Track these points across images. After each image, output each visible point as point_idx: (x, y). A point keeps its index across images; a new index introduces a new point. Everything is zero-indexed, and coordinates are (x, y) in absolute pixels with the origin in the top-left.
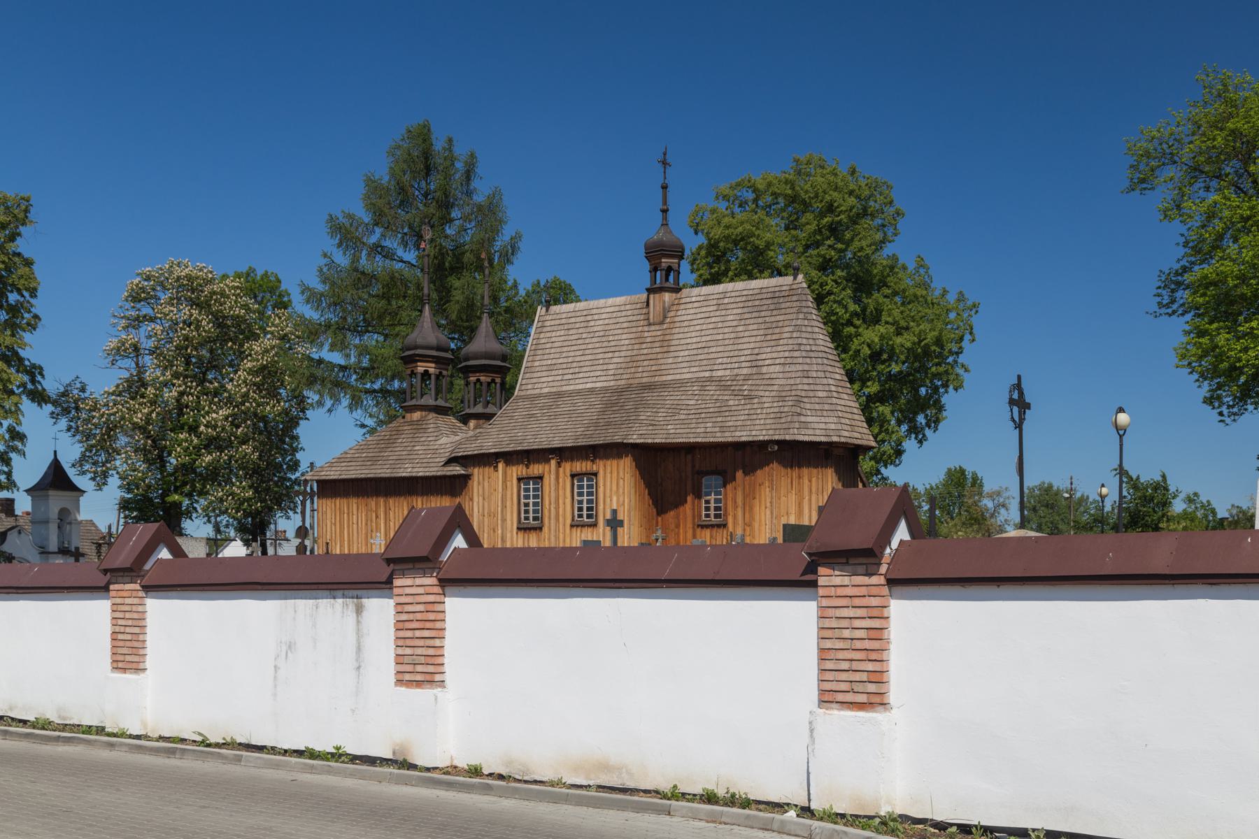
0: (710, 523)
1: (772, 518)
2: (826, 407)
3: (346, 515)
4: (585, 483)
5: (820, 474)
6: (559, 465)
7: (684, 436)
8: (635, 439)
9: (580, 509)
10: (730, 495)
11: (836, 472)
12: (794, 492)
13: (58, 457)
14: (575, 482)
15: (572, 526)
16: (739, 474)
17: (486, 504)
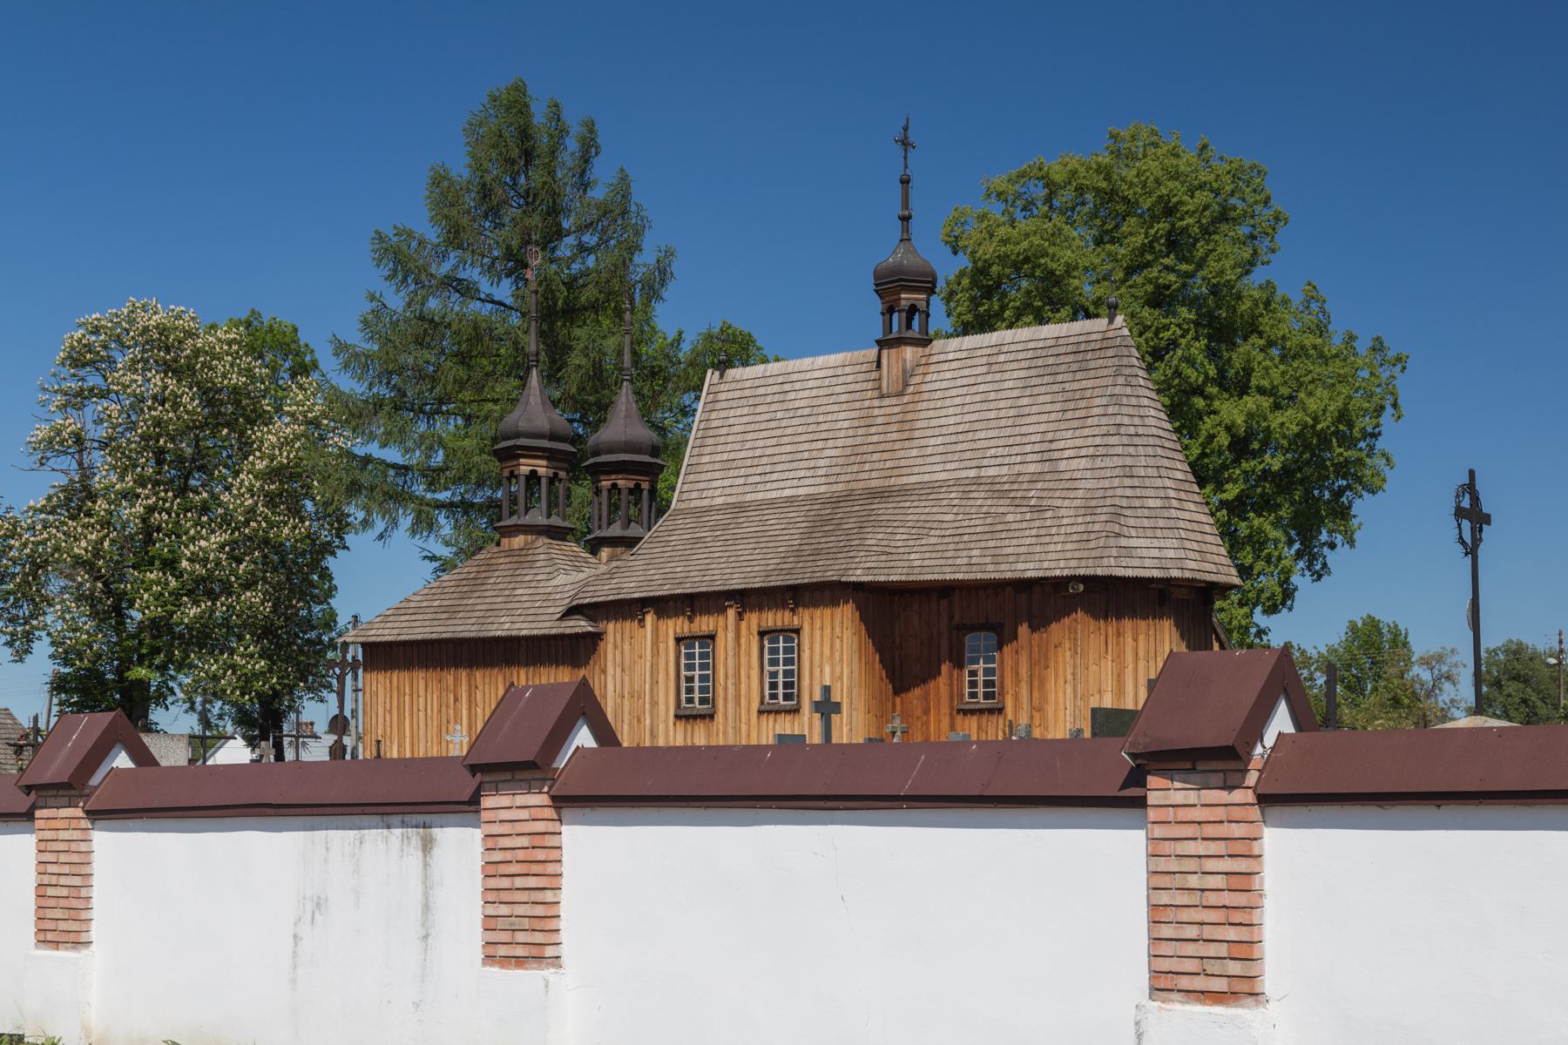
0: (977, 707)
1: (1075, 697)
2: (1161, 523)
3: (407, 697)
4: (781, 645)
5: (1152, 628)
6: (740, 616)
9: (774, 686)
10: (1008, 662)
11: (1177, 625)
12: (1110, 658)
15: (760, 712)
16: (1023, 630)
17: (626, 678)
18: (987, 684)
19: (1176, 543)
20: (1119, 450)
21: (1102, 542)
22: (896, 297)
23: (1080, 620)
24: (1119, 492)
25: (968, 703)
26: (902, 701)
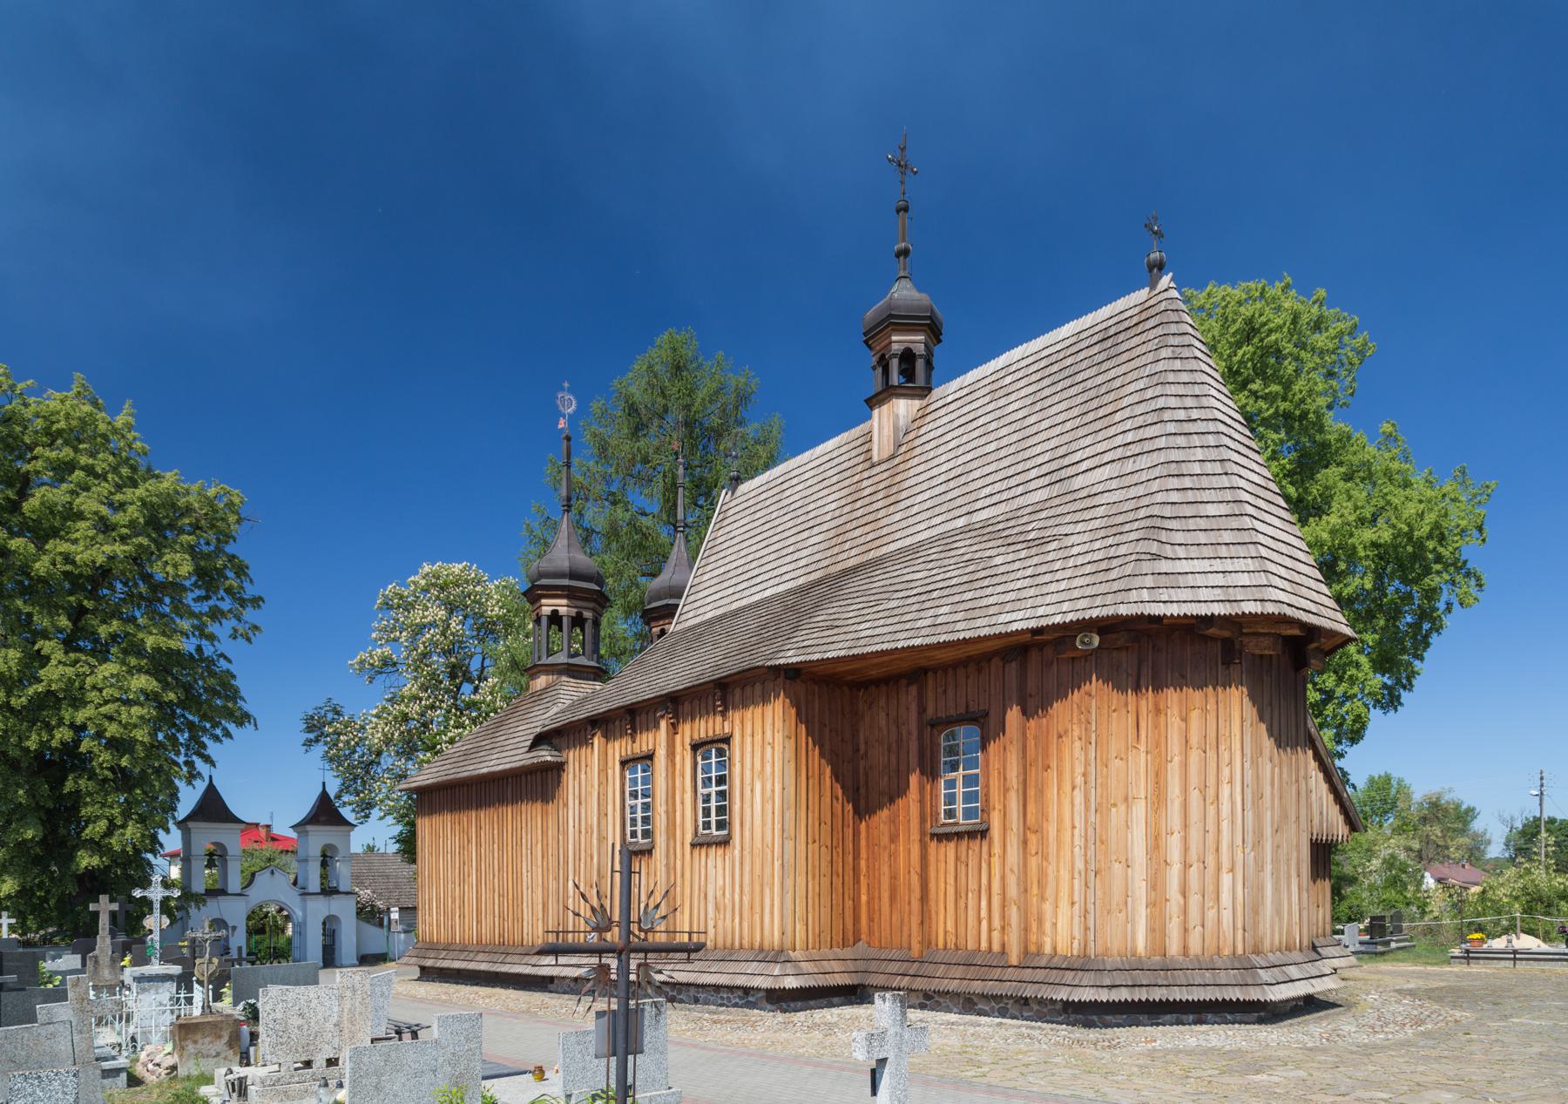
0: (955, 829)
1: (1087, 809)
2: (1227, 537)
5: (1212, 700)
6: (674, 728)
7: (888, 637)
8: (791, 657)
9: (707, 812)
10: (995, 764)
11: (1253, 698)
12: (1143, 748)
13: (215, 783)
14: (699, 759)
15: (693, 845)
16: (1013, 715)
17: (583, 811)
18: (968, 798)
19: (1251, 565)
20: (1161, 443)
21: (1129, 570)
22: (887, 342)
23: (1095, 696)
24: (1159, 498)
25: (944, 825)
26: (868, 827)
